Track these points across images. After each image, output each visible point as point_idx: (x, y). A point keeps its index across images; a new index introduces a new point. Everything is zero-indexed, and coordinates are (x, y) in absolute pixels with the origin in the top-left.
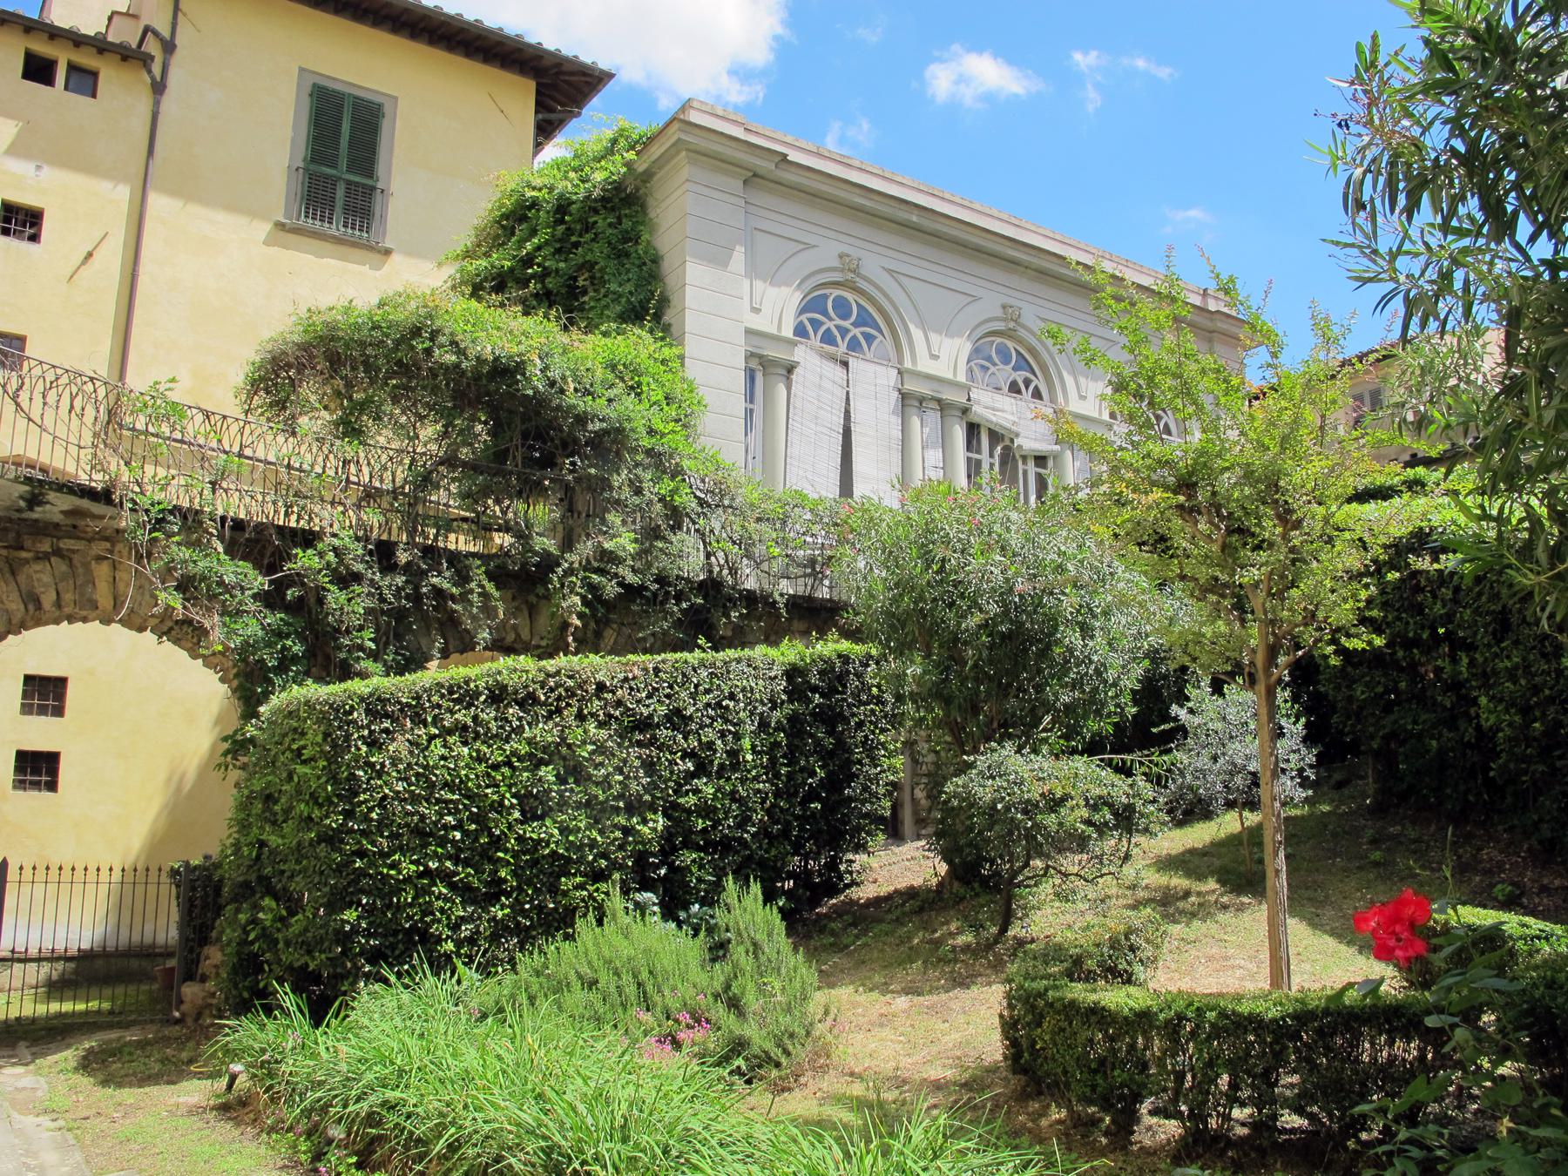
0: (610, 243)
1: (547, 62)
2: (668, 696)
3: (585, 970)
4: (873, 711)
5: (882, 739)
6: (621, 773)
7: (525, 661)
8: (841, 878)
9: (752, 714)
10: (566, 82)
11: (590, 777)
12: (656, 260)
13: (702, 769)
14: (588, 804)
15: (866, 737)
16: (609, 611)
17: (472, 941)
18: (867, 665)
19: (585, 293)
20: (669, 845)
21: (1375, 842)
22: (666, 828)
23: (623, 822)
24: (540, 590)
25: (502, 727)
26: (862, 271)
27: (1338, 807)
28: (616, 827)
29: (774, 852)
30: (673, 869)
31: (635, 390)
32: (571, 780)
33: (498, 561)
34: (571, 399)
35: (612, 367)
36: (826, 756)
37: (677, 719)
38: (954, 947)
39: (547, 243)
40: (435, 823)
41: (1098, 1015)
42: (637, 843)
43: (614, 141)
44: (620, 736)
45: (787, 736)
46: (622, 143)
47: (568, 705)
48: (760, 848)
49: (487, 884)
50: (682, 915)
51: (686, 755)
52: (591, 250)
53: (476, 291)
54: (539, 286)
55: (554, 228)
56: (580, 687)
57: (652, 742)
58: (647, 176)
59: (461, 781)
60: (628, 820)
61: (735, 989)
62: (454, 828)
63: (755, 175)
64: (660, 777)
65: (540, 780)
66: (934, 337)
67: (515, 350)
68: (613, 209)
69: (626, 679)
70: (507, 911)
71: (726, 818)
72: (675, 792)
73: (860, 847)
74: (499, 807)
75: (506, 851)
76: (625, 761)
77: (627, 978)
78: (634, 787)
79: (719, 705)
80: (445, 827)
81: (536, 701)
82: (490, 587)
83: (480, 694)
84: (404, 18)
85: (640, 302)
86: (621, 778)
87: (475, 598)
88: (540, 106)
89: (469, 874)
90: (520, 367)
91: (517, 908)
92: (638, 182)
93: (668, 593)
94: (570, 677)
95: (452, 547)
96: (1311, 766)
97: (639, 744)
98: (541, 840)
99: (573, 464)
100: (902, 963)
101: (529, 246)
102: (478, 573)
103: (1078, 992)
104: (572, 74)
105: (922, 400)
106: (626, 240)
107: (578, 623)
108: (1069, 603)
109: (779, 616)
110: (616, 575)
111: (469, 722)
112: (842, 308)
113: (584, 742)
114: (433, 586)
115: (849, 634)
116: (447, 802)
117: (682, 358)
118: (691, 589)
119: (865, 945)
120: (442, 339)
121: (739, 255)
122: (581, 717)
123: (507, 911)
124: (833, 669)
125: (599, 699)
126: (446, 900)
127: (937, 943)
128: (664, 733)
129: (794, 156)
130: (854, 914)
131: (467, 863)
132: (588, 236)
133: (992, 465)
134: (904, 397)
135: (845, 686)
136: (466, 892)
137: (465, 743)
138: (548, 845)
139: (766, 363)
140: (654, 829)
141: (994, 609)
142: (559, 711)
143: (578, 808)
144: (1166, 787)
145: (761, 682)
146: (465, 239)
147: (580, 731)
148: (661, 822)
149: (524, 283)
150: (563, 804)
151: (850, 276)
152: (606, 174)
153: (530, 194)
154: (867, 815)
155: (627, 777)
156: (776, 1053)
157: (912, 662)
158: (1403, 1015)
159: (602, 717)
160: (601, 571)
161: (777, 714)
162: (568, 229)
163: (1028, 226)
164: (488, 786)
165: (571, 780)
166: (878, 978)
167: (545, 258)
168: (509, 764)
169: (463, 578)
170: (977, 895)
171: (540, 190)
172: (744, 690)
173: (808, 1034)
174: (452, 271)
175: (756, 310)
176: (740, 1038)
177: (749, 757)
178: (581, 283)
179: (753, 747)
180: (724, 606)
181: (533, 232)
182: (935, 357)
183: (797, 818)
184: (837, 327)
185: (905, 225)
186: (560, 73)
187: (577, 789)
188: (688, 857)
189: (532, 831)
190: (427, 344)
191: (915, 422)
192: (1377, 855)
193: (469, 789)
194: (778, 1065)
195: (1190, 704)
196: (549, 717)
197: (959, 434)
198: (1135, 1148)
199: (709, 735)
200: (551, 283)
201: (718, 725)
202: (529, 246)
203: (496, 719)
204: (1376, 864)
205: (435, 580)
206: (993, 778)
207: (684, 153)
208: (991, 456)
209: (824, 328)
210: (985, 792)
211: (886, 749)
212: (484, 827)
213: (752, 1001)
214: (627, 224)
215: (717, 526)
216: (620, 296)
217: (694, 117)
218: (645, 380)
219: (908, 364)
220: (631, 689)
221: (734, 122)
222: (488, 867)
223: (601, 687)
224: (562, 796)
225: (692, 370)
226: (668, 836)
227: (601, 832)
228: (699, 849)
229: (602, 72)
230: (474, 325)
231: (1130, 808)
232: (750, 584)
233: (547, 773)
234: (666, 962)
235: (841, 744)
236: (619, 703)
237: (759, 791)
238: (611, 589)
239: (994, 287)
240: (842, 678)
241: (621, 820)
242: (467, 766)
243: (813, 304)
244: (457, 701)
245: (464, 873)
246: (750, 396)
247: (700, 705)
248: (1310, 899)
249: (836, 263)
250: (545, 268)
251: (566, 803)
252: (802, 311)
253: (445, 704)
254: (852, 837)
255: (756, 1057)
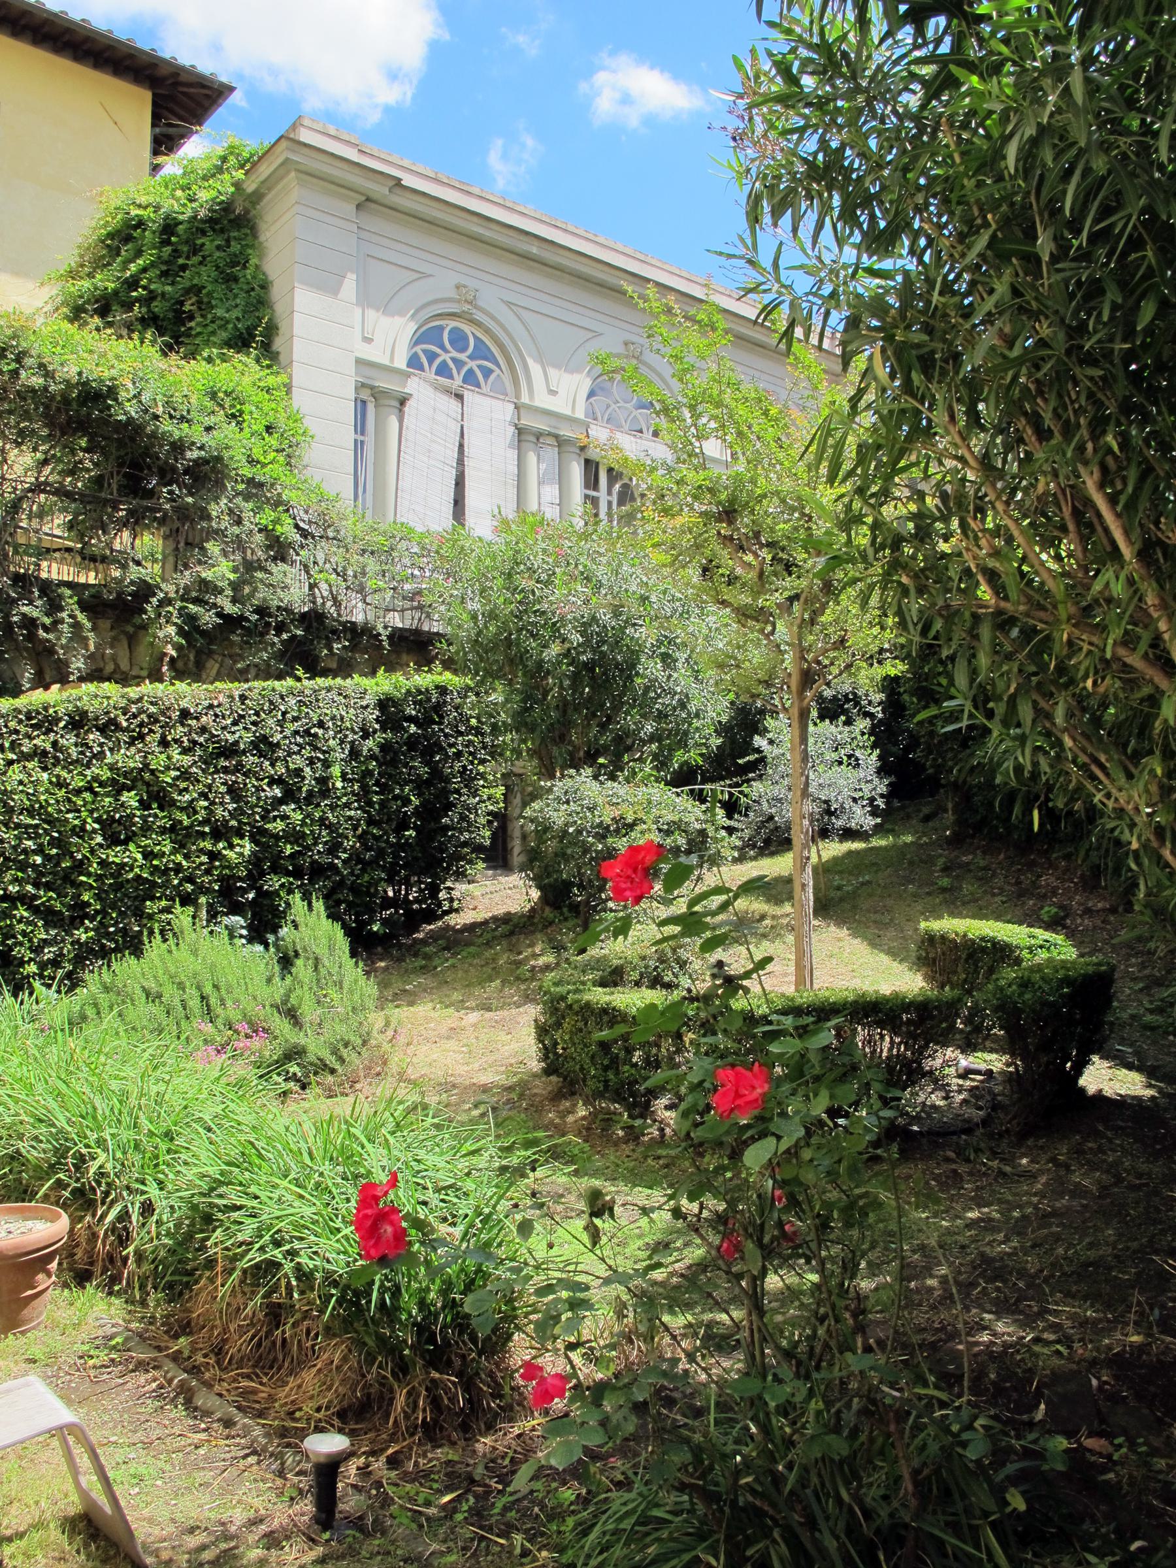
0: (217, 267)
1: (163, 71)
2: (254, 723)
3: (152, 985)
4: (470, 742)
5: (481, 768)
6: (207, 799)
7: (109, 688)
8: (440, 905)
9: (342, 742)
10: (184, 94)
11: (173, 803)
12: (265, 286)
13: (290, 795)
14: (173, 829)
15: (464, 767)
16: (211, 642)
17: (56, 963)
18: (466, 697)
19: (191, 318)
20: (256, 868)
21: (946, 869)
22: (253, 853)
23: (209, 847)
24: (137, 620)
25: (82, 753)
26: (480, 303)
27: (920, 838)
28: (202, 851)
29: (366, 878)
30: (261, 893)
31: (235, 417)
32: (155, 805)
33: (93, 591)
34: (166, 426)
35: (213, 395)
36: (420, 785)
37: (264, 746)
38: (534, 967)
39: (153, 265)
40: (15, 848)
41: (610, 1016)
42: (223, 867)
43: (224, 159)
44: (205, 762)
45: (380, 765)
46: (232, 161)
47: (151, 731)
48: (352, 874)
49: (70, 908)
50: (271, 938)
51: (272, 782)
52: (198, 274)
53: (77, 314)
54: (144, 310)
55: (159, 249)
56: (163, 713)
57: (239, 767)
58: (257, 197)
59: (41, 807)
60: (214, 845)
61: (293, 1001)
62: (35, 852)
63: (368, 199)
64: (247, 803)
65: (122, 805)
66: (553, 372)
67: (106, 374)
68: (222, 231)
69: (211, 706)
70: (91, 934)
71: (316, 844)
72: (263, 818)
73: (460, 875)
74: (81, 832)
75: (89, 875)
76: (210, 787)
77: (192, 993)
78: (219, 812)
79: (307, 732)
80: (25, 851)
81: (118, 727)
82: (81, 617)
83: (60, 719)
84: (46, 29)
85: (248, 329)
86: (206, 804)
87: (65, 628)
88: (156, 118)
89: (51, 898)
90: (112, 392)
91: (102, 930)
92: (247, 204)
93: (268, 624)
94: (152, 703)
95: (44, 575)
96: (882, 796)
97: (226, 770)
98: (126, 864)
99: (171, 492)
100: (483, 981)
101: (133, 267)
102: (70, 601)
103: (599, 996)
104: (191, 85)
105: (539, 435)
106: (234, 264)
107: (174, 653)
108: (646, 634)
109: (380, 647)
110: (215, 605)
111: (49, 748)
112: (459, 340)
113: (168, 768)
114: (24, 615)
115: (448, 665)
116: (27, 826)
117: (288, 388)
118: (292, 621)
119: (453, 966)
120: (29, 362)
121: (350, 284)
122: (164, 743)
123: (91, 934)
124: (429, 700)
125: (183, 725)
126: (29, 923)
127: (518, 964)
128: (250, 760)
129: (409, 181)
130: (448, 939)
131: (48, 887)
132: (195, 259)
133: (610, 503)
134: (521, 431)
135: (441, 717)
136: (50, 917)
137: (45, 769)
138: (132, 870)
139: (378, 395)
140: (241, 854)
141: (576, 638)
142: (141, 737)
143: (162, 833)
144: (746, 815)
145: (352, 711)
146: (70, 258)
147: (163, 756)
148: (247, 847)
149: (128, 306)
150: (146, 829)
151: (466, 307)
152: (214, 193)
153: (135, 212)
154: (465, 844)
155: (213, 803)
156: (331, 1061)
157: (495, 690)
158: (880, 1011)
159: (186, 744)
160: (197, 601)
161: (370, 743)
162: (175, 251)
163: (653, 262)
164: (68, 811)
165: (155, 805)
166: (456, 996)
167: (150, 281)
168: (90, 789)
169: (54, 606)
170: (566, 919)
171: (145, 208)
172: (333, 718)
173: (365, 1043)
174: (54, 292)
175: (368, 340)
176: (295, 1046)
177: (339, 784)
178: (187, 308)
179: (344, 776)
180: (327, 638)
181: (139, 253)
182: (553, 393)
183: (392, 845)
184: (454, 360)
185: (526, 257)
186: (176, 84)
187: (161, 815)
188: (274, 882)
189: (115, 856)
190: (14, 366)
191: (532, 458)
192: (945, 882)
193: (51, 815)
194: (333, 1071)
195: (770, 735)
196: (131, 743)
197: (576, 471)
198: (646, 1139)
199: (297, 762)
200: (157, 306)
201: (306, 752)
202: (133, 267)
203: (76, 745)
204: (944, 890)
205: (25, 609)
206: (568, 802)
207: (293, 174)
208: (609, 493)
209: (465, 369)
210: (558, 817)
211: (486, 780)
212: (66, 852)
213: (309, 1012)
214: (235, 247)
215: (320, 557)
216: (228, 322)
217: (305, 136)
218: (247, 408)
219: (525, 399)
220: (216, 716)
221: (348, 143)
222: (71, 891)
223: (185, 714)
224: (145, 821)
225: (300, 400)
226: (255, 861)
227: (187, 857)
228: (288, 874)
229: (222, 85)
230: (63, 347)
231: (702, 833)
232: (358, 617)
233: (130, 799)
234: (229, 977)
235: (436, 773)
236: (204, 730)
237: (350, 818)
238: (208, 619)
239: (617, 323)
240: (438, 708)
241: (207, 845)
242: (47, 791)
243: (427, 336)
244: (35, 727)
245: (45, 897)
246: (360, 426)
247: (288, 733)
248: (875, 922)
249: (453, 294)
250: (151, 292)
251: (150, 828)
252: (416, 343)
253: (22, 729)
254: (450, 865)
255: (312, 1064)
